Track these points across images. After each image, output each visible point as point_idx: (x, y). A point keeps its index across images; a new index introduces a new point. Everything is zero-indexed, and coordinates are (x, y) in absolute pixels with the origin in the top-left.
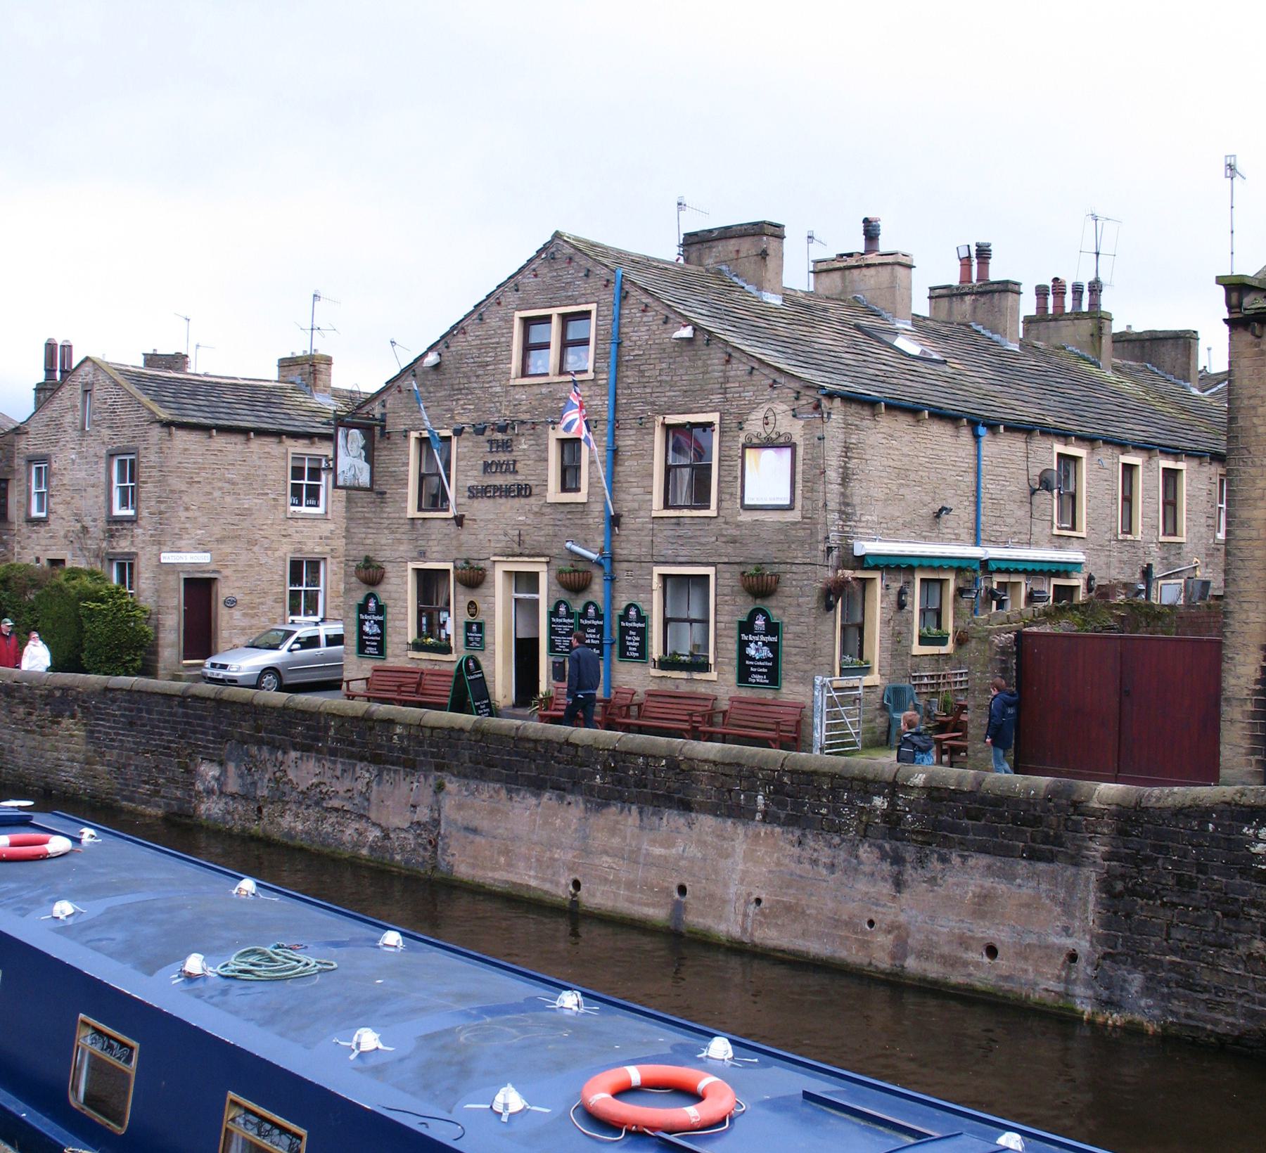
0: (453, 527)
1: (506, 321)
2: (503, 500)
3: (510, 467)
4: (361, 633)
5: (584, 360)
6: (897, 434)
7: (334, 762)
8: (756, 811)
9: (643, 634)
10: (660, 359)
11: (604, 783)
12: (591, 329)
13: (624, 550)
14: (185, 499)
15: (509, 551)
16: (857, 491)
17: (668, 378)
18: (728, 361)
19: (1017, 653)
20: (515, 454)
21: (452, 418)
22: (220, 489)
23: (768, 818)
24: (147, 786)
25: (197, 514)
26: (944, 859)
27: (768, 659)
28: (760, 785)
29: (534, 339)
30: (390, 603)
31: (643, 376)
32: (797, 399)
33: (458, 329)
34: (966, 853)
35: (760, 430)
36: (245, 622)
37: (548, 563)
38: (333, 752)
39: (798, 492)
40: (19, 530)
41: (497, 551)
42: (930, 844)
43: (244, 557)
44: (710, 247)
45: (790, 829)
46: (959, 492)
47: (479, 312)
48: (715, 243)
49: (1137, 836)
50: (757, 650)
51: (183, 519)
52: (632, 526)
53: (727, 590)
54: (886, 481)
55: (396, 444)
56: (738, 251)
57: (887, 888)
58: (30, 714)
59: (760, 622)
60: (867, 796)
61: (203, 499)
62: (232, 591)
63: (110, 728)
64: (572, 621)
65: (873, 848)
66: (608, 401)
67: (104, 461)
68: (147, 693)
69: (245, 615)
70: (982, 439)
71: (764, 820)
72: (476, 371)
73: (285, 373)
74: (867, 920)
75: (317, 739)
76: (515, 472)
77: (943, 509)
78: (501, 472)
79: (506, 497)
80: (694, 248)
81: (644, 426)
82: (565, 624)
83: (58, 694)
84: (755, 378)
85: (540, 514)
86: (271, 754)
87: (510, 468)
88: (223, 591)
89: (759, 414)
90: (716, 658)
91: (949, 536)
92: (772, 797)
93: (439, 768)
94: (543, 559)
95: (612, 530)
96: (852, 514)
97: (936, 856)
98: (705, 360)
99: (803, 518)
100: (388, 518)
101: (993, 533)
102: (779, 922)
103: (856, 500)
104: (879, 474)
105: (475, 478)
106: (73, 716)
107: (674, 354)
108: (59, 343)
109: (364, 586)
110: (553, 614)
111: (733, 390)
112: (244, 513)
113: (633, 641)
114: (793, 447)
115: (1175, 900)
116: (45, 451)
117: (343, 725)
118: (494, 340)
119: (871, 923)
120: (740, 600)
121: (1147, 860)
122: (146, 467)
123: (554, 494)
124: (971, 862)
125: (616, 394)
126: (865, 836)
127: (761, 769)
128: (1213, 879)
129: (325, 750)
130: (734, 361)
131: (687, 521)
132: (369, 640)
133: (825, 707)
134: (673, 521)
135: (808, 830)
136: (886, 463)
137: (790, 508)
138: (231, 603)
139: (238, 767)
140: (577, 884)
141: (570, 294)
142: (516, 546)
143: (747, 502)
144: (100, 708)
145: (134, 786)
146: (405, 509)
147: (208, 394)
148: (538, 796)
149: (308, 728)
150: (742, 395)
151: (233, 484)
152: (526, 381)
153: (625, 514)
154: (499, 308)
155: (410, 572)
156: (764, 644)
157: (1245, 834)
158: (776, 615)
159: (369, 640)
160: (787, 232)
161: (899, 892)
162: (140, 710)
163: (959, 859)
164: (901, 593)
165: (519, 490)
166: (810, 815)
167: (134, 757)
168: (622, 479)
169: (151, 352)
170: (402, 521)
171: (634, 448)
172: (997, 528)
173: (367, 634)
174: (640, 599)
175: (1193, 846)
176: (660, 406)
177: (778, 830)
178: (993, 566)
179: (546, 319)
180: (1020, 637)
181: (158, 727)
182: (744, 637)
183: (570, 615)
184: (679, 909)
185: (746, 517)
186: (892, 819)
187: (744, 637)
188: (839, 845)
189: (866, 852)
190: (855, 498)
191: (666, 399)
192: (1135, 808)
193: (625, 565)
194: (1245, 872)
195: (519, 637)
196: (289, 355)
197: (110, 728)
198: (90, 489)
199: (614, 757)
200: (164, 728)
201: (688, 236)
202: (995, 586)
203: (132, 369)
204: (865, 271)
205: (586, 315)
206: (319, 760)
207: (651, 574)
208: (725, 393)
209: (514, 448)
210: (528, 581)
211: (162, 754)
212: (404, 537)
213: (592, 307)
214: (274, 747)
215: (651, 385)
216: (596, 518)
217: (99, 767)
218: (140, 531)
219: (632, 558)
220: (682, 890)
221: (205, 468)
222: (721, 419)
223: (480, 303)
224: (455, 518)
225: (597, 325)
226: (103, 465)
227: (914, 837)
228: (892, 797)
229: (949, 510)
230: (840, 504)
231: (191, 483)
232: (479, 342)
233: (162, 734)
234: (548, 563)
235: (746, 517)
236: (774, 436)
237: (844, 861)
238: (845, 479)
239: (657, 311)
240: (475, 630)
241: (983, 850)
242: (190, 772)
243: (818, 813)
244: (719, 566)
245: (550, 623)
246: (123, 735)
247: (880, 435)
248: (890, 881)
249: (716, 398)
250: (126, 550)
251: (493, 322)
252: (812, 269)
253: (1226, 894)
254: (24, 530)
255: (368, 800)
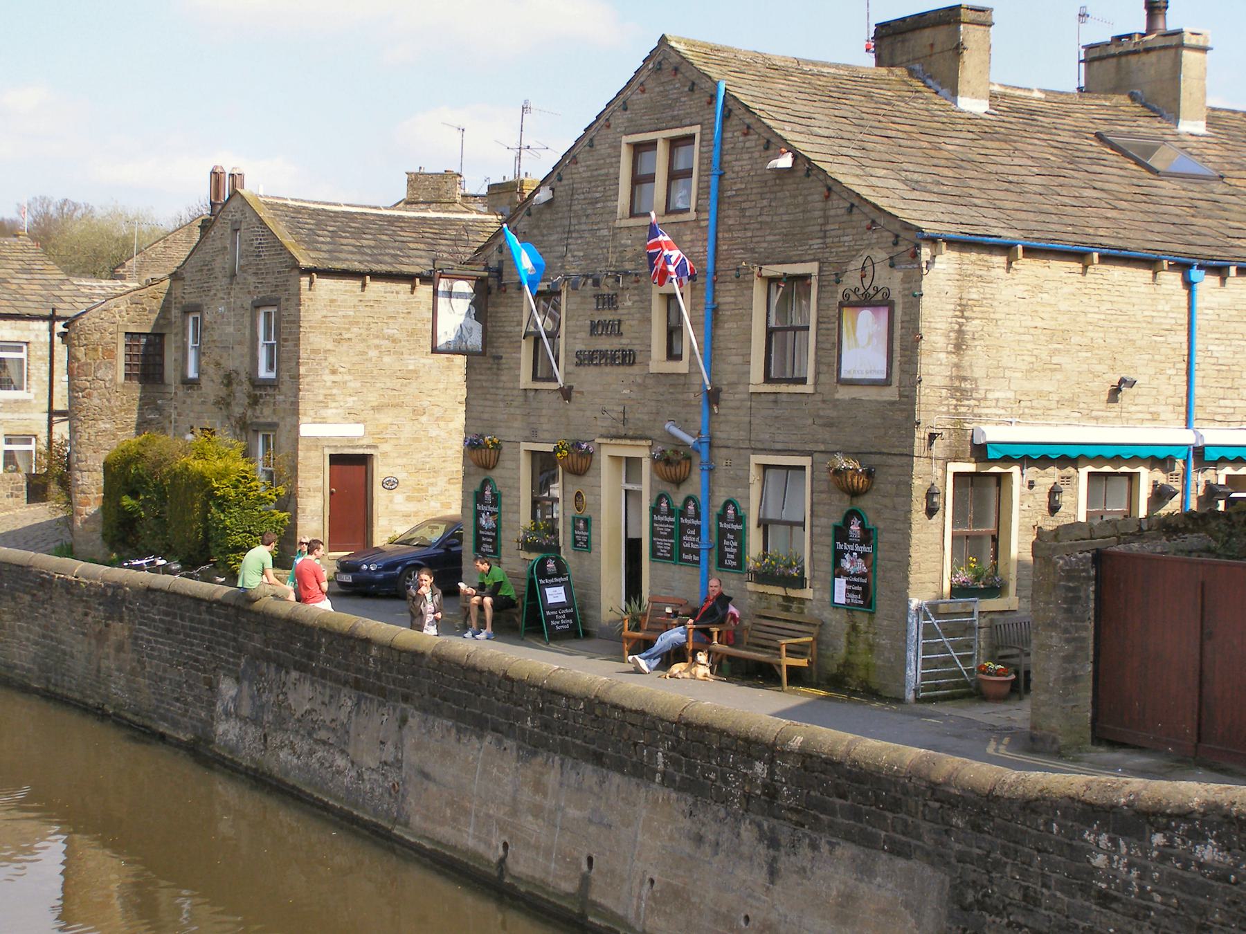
0: (556, 401)
1: (615, 147)
2: (608, 369)
3: (614, 328)
4: (478, 527)
5: (688, 195)
6: (1047, 286)
7: (324, 686)
8: (655, 772)
9: (741, 536)
10: (761, 194)
11: (533, 727)
12: (693, 157)
13: (721, 435)
14: (331, 359)
15: (613, 431)
16: (978, 361)
17: (768, 219)
18: (827, 197)
19: (1097, 578)
20: (620, 311)
21: (562, 267)
22: (377, 347)
23: (667, 780)
24: (178, 704)
25: (347, 377)
26: (814, 846)
27: (863, 575)
28: (660, 740)
29: (680, 165)
30: (504, 491)
31: (744, 216)
32: (896, 244)
33: (570, 157)
34: (834, 840)
35: (858, 284)
36: (411, 507)
37: (650, 447)
38: (324, 674)
39: (896, 364)
40: (176, 393)
41: (603, 431)
42: (803, 826)
43: (408, 430)
44: (903, 41)
45: (684, 796)
46: (1157, 357)
47: (589, 138)
48: (909, 35)
49: (989, 833)
50: (852, 562)
51: (329, 384)
52: (731, 404)
53: (824, 486)
54: (1030, 346)
55: (512, 297)
56: (932, 45)
57: (761, 876)
58: (86, 614)
59: (855, 528)
60: (750, 759)
61: (356, 359)
62: (392, 470)
63: (151, 634)
64: (673, 520)
65: (754, 826)
66: (710, 249)
67: (248, 314)
68: (175, 593)
69: (409, 499)
70: (1197, 286)
71: (662, 783)
72: (585, 210)
73: (494, 203)
74: (743, 915)
75: (311, 658)
76: (620, 334)
77: (1122, 381)
78: (607, 334)
79: (612, 365)
80: (887, 41)
81: (741, 278)
82: (665, 523)
83: (110, 592)
84: (855, 218)
85: (643, 387)
86: (276, 675)
87: (614, 328)
88: (380, 471)
89: (858, 264)
90: (812, 570)
91: (1140, 416)
92: (671, 754)
93: (406, 698)
94: (643, 443)
95: (711, 409)
96: (972, 390)
97: (807, 841)
98: (806, 196)
99: (900, 396)
100: (504, 388)
101: (1219, 410)
102: (668, 911)
103: (978, 372)
104: (1018, 337)
105: (583, 343)
106: (121, 620)
107: (776, 188)
108: (228, 171)
109: (481, 470)
110: (655, 511)
111: (833, 233)
112: (408, 376)
113: (731, 548)
114: (888, 303)
115: (1021, 920)
116: (198, 301)
117: (332, 643)
118: (603, 172)
119: (747, 919)
120: (836, 497)
121: (998, 865)
122: (287, 322)
123: (657, 361)
124: (838, 851)
125: (717, 238)
126: (747, 810)
127: (662, 720)
128: (1055, 896)
129: (317, 671)
130: (834, 197)
131: (784, 398)
132: (485, 536)
133: (921, 637)
134: (772, 397)
135: (699, 798)
136: (1030, 324)
137: (886, 383)
138: (391, 484)
139: (250, 686)
140: (505, 846)
141: (676, 113)
142: (621, 425)
143: (844, 375)
144: (143, 612)
145: (168, 704)
146: (517, 378)
147: (359, 233)
148: (480, 737)
149: (306, 644)
150: (842, 239)
151: (394, 341)
152: (672, 218)
153: (725, 388)
154: (609, 131)
155: (522, 454)
156: (860, 555)
157: (1086, 841)
158: (871, 520)
159: (485, 536)
160: (995, 17)
161: (772, 883)
162: (175, 616)
163: (827, 847)
164: (1054, 492)
165: (624, 357)
166: (701, 779)
167: (169, 670)
168: (722, 345)
169: (417, 170)
170: (515, 392)
171: (733, 307)
172: (1227, 403)
173: (483, 529)
174: (736, 494)
175: (1039, 851)
176: (761, 253)
177: (674, 795)
178: (1211, 455)
179: (652, 145)
180: (1099, 558)
181: (189, 636)
182: (840, 546)
183: (671, 513)
184: (585, 881)
185: (843, 394)
186: (771, 791)
187: (840, 546)
188: (724, 819)
189: (746, 830)
190: (975, 369)
191: (765, 245)
192: (987, 796)
193: (724, 452)
194: (1085, 889)
195: (629, 537)
196: (501, 181)
197: (151, 634)
198: (236, 347)
199: (542, 695)
200: (195, 637)
201: (881, 27)
202: (1222, 481)
203: (290, 203)
204: (1145, 58)
205: (691, 138)
206: (312, 684)
207: (748, 464)
208: (825, 237)
209: (619, 304)
210: (632, 465)
211: (192, 667)
212: (518, 412)
213: (696, 130)
214: (280, 666)
215: (752, 227)
216: (695, 397)
217: (141, 679)
218: (281, 398)
219: (730, 443)
220: (590, 860)
221: (357, 323)
222: (820, 269)
223: (591, 126)
224: (561, 389)
225: (700, 152)
226: (247, 320)
227: (790, 816)
228: (771, 762)
229: (1132, 384)
230: (951, 378)
231: (338, 341)
232: (589, 174)
233: (192, 645)
234: (650, 447)
235: (843, 394)
236: (871, 292)
237: (727, 840)
238: (959, 345)
239: (759, 135)
240: (584, 525)
241: (849, 837)
242: (212, 687)
243: (708, 778)
244: (816, 455)
245: (653, 521)
246: (162, 644)
247: (1021, 287)
248: (765, 868)
249: (816, 243)
250: (269, 420)
251: (603, 149)
252: (1082, 58)
253: (1067, 917)
254: (180, 393)
255: (347, 732)
